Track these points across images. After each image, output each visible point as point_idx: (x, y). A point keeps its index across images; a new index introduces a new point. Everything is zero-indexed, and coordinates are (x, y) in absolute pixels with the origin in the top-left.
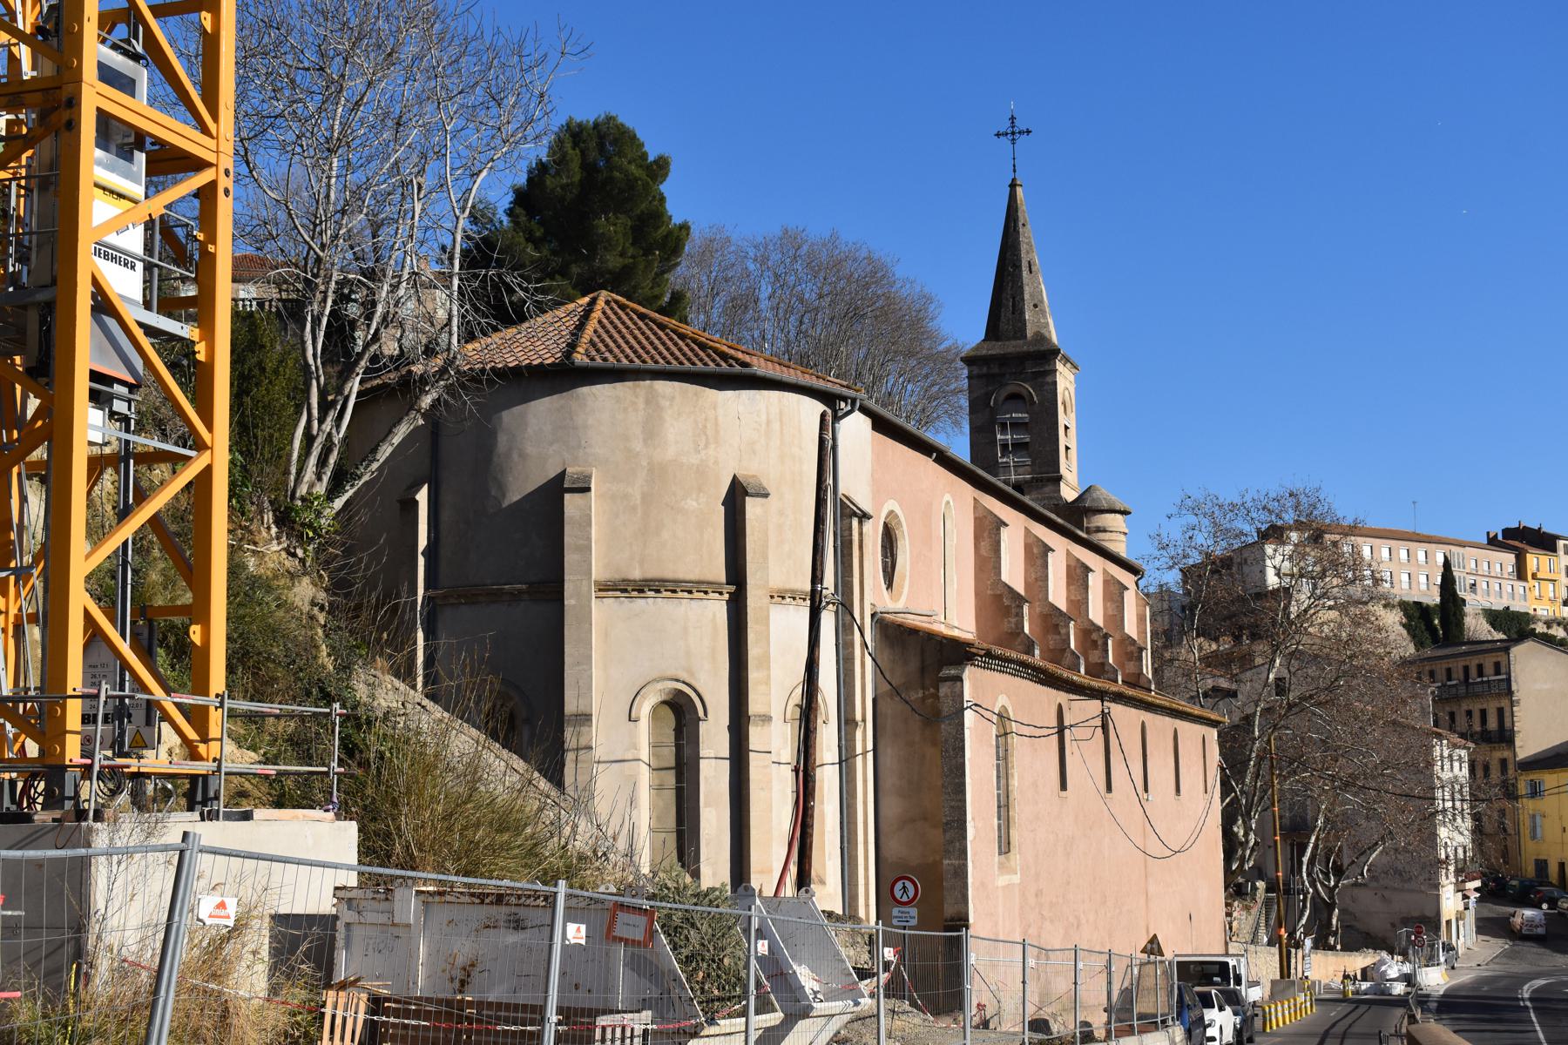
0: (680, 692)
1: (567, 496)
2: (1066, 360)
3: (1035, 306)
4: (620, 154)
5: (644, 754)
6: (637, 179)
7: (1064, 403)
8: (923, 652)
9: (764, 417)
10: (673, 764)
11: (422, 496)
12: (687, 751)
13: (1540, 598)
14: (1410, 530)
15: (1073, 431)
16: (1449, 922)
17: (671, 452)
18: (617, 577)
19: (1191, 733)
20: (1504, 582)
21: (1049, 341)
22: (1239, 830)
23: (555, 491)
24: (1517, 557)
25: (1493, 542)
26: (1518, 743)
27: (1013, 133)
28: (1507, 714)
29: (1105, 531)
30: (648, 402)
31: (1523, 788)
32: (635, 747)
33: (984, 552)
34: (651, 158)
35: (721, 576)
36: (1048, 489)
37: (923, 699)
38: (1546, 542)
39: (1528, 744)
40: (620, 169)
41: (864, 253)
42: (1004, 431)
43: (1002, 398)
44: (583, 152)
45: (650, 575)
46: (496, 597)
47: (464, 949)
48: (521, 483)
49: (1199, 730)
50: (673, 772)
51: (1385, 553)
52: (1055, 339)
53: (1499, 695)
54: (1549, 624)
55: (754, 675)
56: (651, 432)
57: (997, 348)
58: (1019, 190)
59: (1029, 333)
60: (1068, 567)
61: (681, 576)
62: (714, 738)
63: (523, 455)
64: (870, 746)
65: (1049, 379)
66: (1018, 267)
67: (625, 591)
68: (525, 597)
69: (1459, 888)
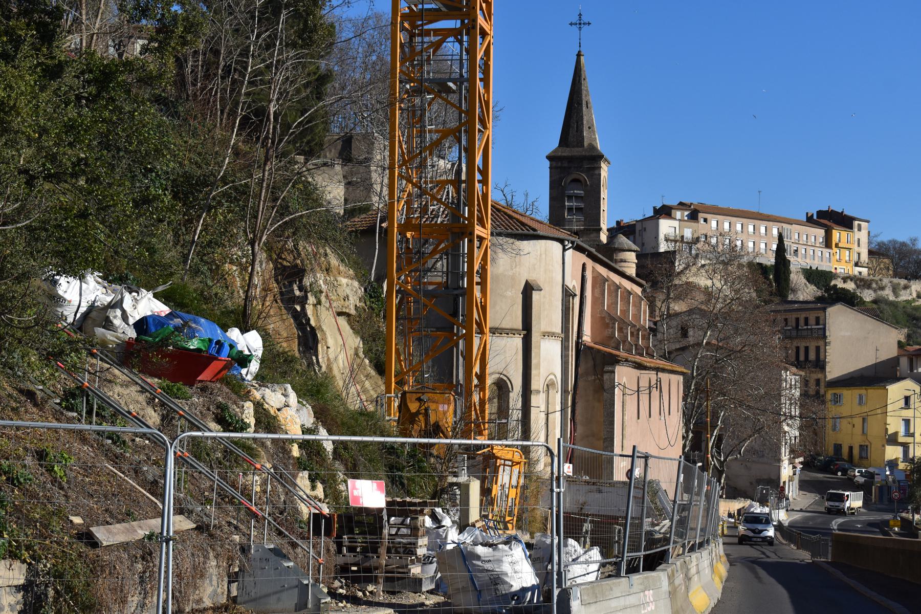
13: (839, 261)
14: (755, 210)
16: (784, 483)
20: (816, 249)
24: (826, 232)
25: (810, 220)
26: (828, 369)
27: (580, 24)
28: (822, 350)
31: (829, 396)
33: (596, 295)
36: (593, 235)
37: (595, 380)
38: (846, 222)
39: (836, 367)
47: (582, 499)
51: (739, 227)
53: (818, 338)
54: (845, 280)
55: (534, 372)
57: (567, 152)
58: (582, 58)
59: (586, 144)
65: (597, 172)
66: (580, 104)
69: (791, 462)
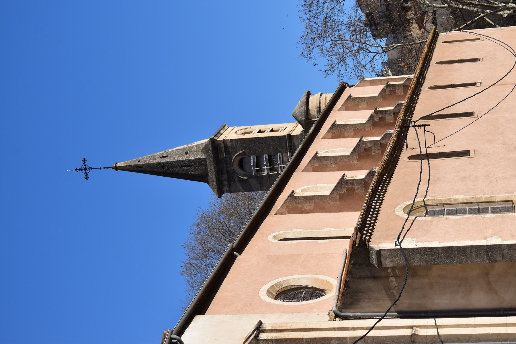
2: (218, 133)
3: (186, 153)
7: (244, 134)
8: (360, 278)
15: (262, 127)
19: (441, 52)
21: (206, 144)
22: (506, 13)
27: (85, 169)
29: (320, 107)
33: (311, 207)
37: (396, 276)
41: (196, 228)
42: (263, 170)
43: (242, 172)
49: (439, 45)
52: (206, 141)
57: (212, 176)
58: (119, 165)
59: (203, 156)
60: (332, 138)
64: (431, 321)
65: (229, 144)
66: (163, 165)
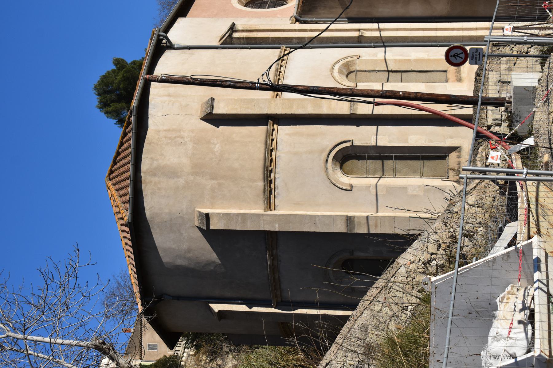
0: (335, 157)
1: (212, 227)
4: (112, 83)
5: (372, 181)
6: (124, 76)
9: (166, 98)
10: (379, 162)
11: (216, 307)
12: (372, 153)
17: (185, 161)
18: (262, 196)
23: (210, 234)
30: (154, 175)
32: (368, 187)
34: (114, 67)
35: (263, 129)
40: (119, 84)
44: (112, 102)
45: (261, 176)
46: (275, 269)
48: (206, 253)
50: (385, 162)
56: (172, 173)
61: (262, 156)
62: (364, 136)
63: (189, 251)
64: (375, 26)
67: (270, 192)
68: (275, 252)
